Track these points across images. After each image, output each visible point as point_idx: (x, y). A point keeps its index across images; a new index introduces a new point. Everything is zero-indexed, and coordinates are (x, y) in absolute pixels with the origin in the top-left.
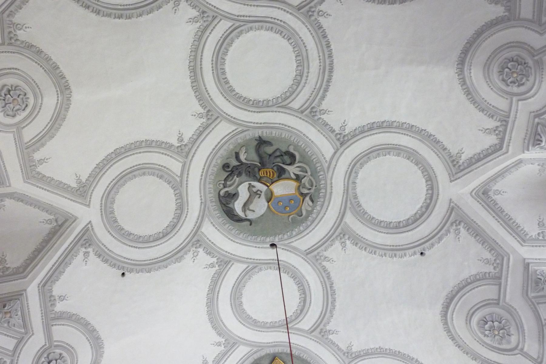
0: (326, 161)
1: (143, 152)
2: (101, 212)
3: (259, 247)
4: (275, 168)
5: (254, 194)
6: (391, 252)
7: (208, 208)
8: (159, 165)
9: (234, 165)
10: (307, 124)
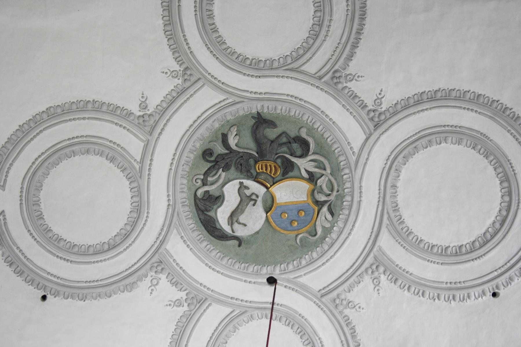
0: (353, 152)
1: (88, 118)
2: (21, 200)
3: (250, 282)
4: (279, 161)
5: (246, 199)
6: (447, 293)
7: (178, 214)
8: (111, 141)
9: (220, 152)
10: (326, 95)
